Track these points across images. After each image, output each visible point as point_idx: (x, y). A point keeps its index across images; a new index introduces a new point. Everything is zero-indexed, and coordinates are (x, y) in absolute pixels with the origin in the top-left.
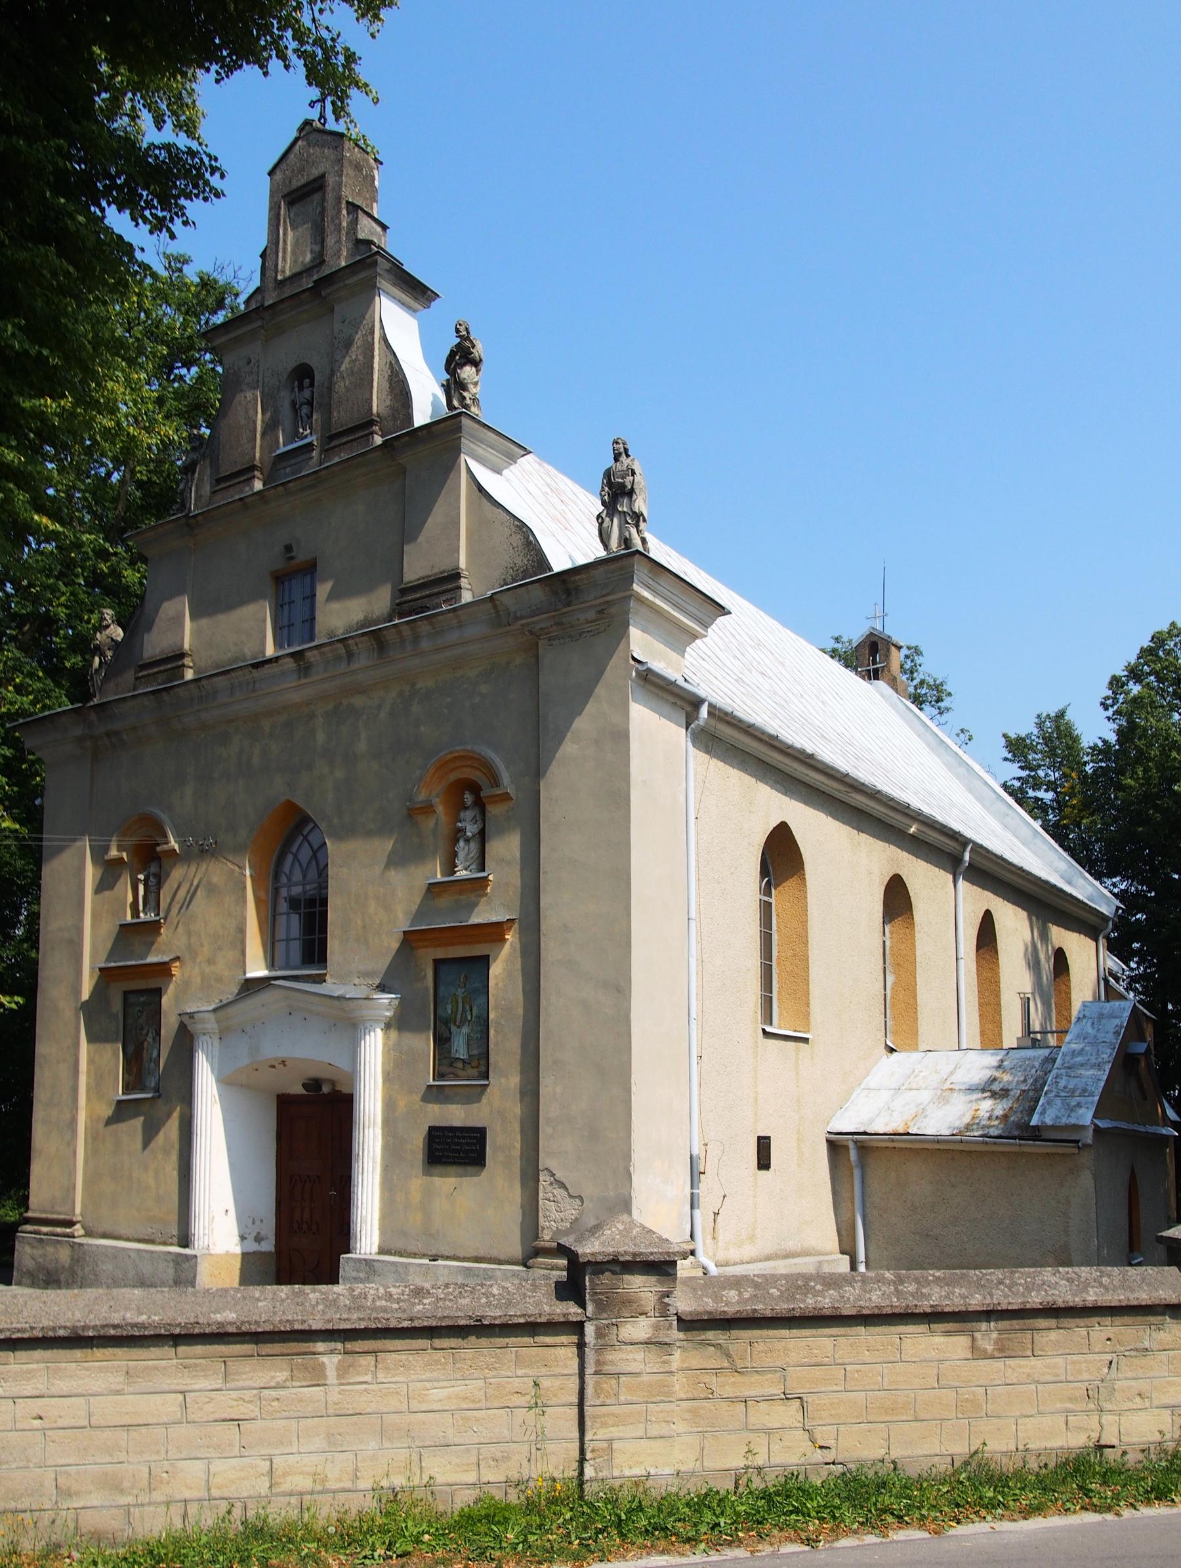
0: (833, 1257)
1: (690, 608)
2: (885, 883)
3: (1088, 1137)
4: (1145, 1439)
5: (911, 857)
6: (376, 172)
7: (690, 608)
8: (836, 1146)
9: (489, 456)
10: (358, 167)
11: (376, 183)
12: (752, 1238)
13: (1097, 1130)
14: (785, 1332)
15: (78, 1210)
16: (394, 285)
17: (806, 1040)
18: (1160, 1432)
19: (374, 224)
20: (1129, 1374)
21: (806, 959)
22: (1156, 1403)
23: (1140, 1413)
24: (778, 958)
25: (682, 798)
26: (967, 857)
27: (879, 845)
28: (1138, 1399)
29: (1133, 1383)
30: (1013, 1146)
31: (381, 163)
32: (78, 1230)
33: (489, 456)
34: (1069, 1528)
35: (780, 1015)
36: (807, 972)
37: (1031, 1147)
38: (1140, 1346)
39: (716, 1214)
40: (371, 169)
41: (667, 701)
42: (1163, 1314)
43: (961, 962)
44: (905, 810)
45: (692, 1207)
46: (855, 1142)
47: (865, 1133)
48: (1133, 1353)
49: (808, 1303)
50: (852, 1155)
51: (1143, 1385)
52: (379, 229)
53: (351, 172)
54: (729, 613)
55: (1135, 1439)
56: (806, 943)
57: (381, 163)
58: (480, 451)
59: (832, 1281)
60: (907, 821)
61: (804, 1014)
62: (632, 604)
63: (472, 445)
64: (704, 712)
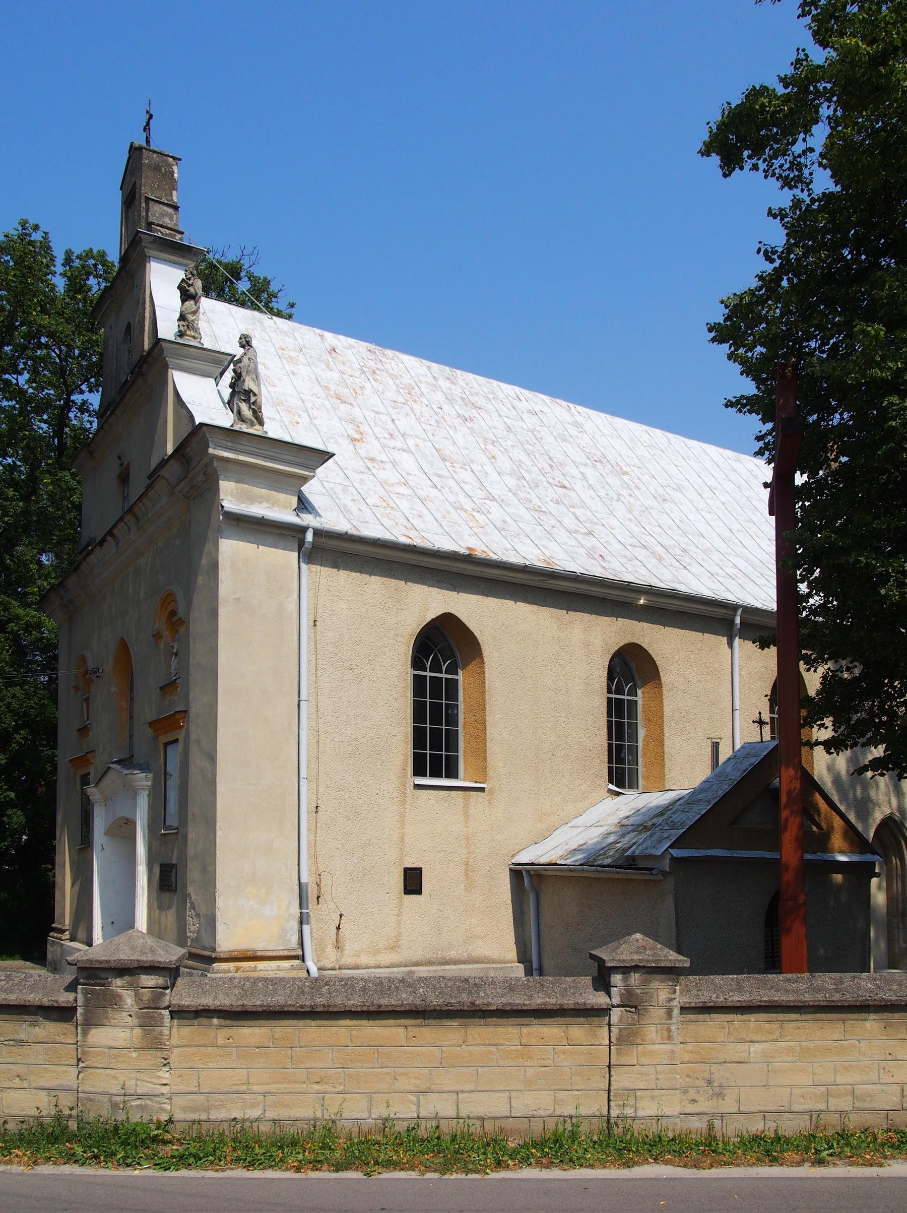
0: (513, 965)
1: (284, 457)
2: (612, 651)
3: (666, 865)
4: (24, 1113)
5: (656, 627)
6: (175, 169)
7: (284, 457)
8: (517, 874)
9: (196, 365)
10: (157, 168)
11: (176, 175)
12: (394, 948)
13: (674, 859)
14: (365, 1022)
15: (67, 921)
16: (161, 251)
17: (482, 790)
18: (38, 1109)
19: (166, 208)
20: (10, 1060)
21: (484, 723)
22: (34, 1085)
23: (20, 1091)
24: (465, 723)
25: (293, 607)
26: (738, 620)
27: (605, 620)
28: (17, 1080)
29: (11, 1066)
30: (613, 874)
31: (180, 160)
32: (67, 935)
33: (196, 365)
34: (55, 1177)
35: (465, 769)
36: (485, 734)
37: (632, 874)
38: (17, 1037)
39: (338, 928)
40: (170, 166)
41: (271, 533)
42: (35, 1014)
43: (737, 713)
44: (629, 587)
45: (301, 923)
46: (528, 871)
47: (532, 864)
48: (11, 1043)
49: (386, 1001)
50: (528, 881)
51: (21, 1069)
52: (170, 211)
53: (150, 174)
54: (329, 455)
55: (15, 1112)
56: (484, 710)
57: (180, 160)
58: (187, 364)
59: (511, 986)
60: (633, 595)
61: (482, 770)
62: (215, 464)
63: (177, 361)
64: (309, 537)
